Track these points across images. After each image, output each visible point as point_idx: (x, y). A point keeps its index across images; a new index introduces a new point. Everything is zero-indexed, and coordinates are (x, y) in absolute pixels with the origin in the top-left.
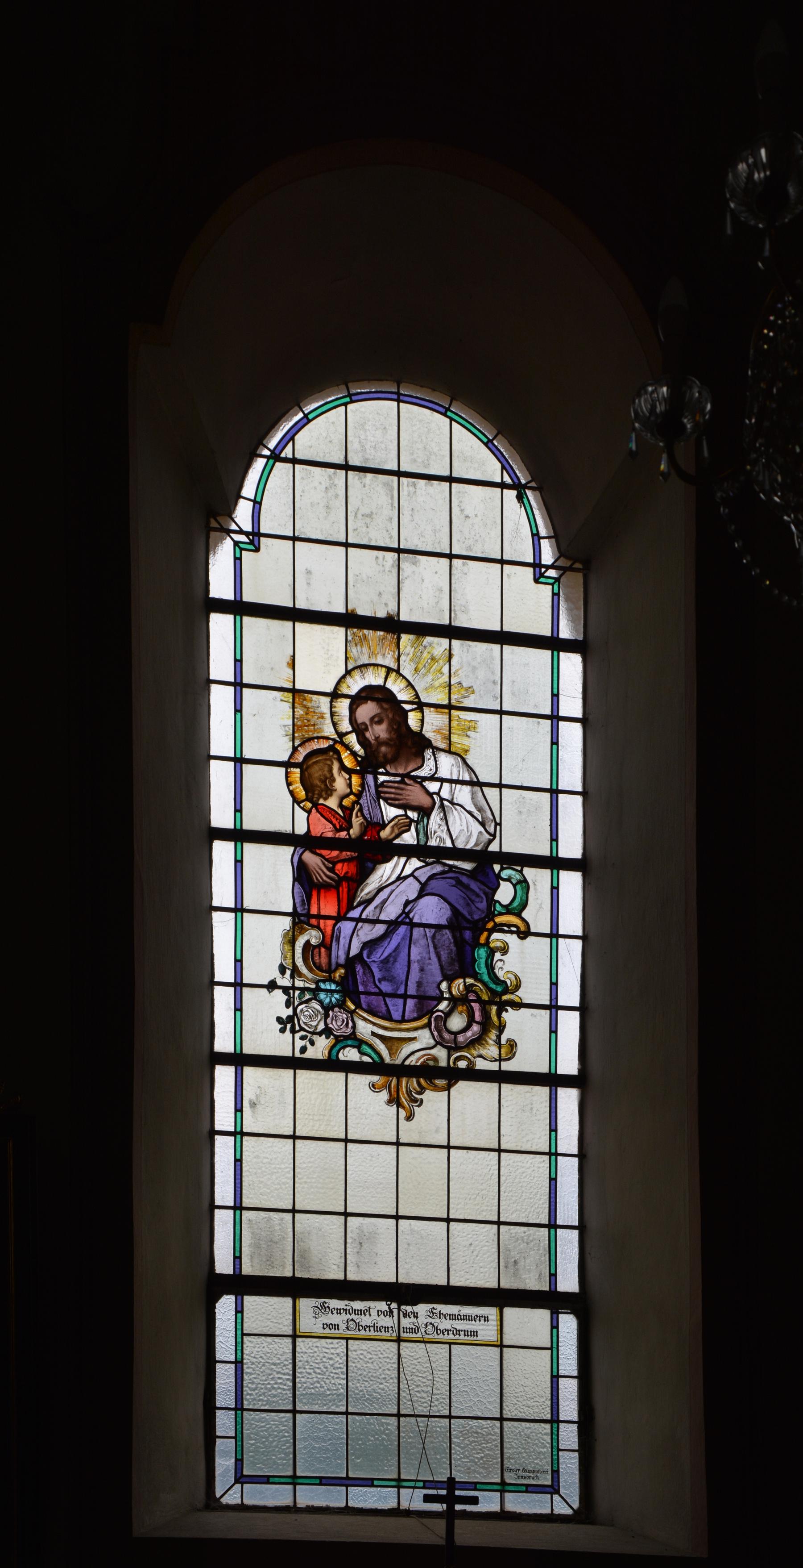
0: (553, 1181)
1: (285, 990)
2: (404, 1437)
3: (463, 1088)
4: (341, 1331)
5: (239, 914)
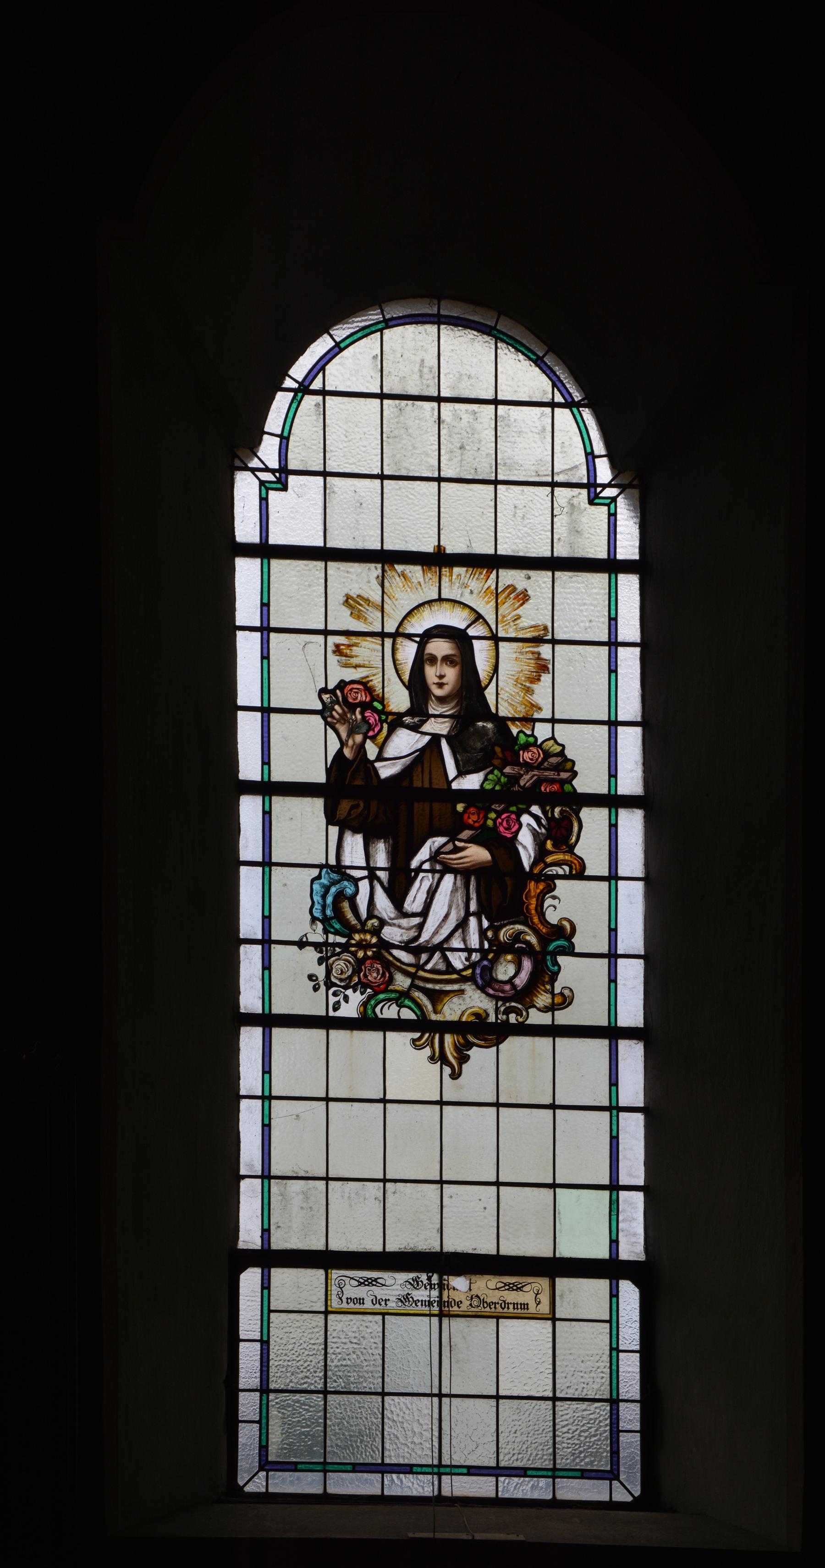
0: (614, 1140)
1: (317, 946)
2: (320, 1418)
3: (513, 1045)
4: (365, 1306)
5: (613, 882)
